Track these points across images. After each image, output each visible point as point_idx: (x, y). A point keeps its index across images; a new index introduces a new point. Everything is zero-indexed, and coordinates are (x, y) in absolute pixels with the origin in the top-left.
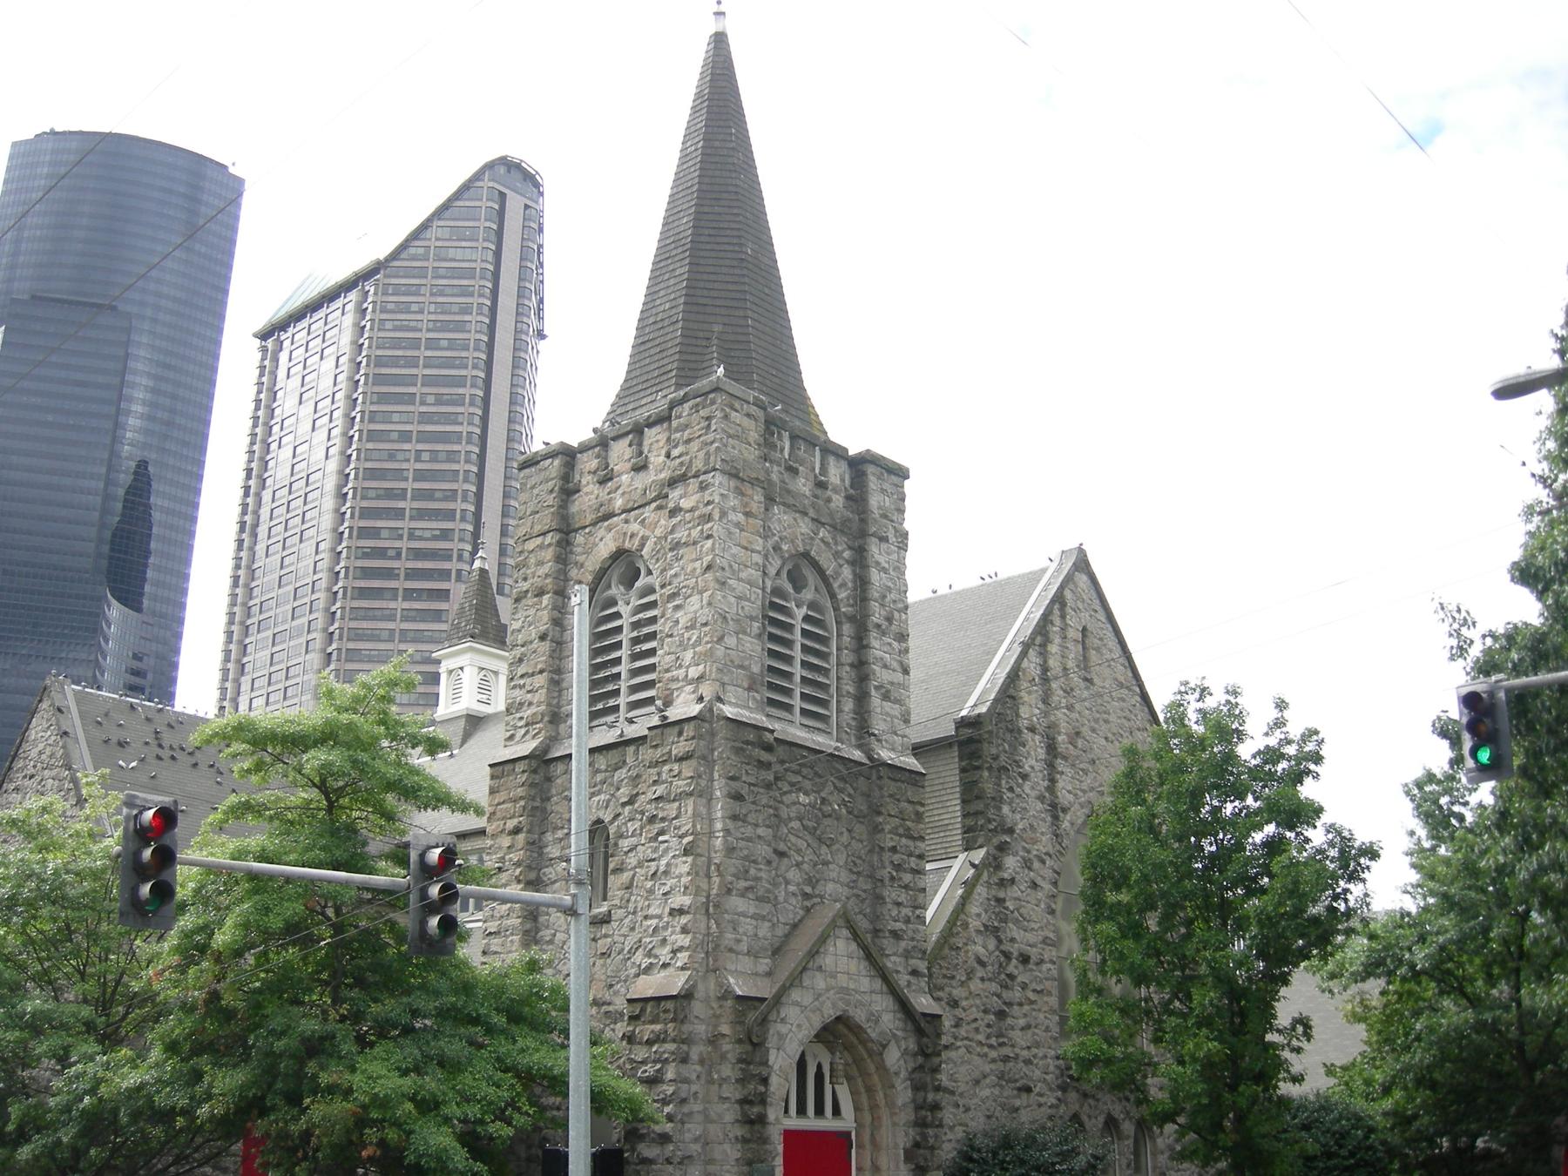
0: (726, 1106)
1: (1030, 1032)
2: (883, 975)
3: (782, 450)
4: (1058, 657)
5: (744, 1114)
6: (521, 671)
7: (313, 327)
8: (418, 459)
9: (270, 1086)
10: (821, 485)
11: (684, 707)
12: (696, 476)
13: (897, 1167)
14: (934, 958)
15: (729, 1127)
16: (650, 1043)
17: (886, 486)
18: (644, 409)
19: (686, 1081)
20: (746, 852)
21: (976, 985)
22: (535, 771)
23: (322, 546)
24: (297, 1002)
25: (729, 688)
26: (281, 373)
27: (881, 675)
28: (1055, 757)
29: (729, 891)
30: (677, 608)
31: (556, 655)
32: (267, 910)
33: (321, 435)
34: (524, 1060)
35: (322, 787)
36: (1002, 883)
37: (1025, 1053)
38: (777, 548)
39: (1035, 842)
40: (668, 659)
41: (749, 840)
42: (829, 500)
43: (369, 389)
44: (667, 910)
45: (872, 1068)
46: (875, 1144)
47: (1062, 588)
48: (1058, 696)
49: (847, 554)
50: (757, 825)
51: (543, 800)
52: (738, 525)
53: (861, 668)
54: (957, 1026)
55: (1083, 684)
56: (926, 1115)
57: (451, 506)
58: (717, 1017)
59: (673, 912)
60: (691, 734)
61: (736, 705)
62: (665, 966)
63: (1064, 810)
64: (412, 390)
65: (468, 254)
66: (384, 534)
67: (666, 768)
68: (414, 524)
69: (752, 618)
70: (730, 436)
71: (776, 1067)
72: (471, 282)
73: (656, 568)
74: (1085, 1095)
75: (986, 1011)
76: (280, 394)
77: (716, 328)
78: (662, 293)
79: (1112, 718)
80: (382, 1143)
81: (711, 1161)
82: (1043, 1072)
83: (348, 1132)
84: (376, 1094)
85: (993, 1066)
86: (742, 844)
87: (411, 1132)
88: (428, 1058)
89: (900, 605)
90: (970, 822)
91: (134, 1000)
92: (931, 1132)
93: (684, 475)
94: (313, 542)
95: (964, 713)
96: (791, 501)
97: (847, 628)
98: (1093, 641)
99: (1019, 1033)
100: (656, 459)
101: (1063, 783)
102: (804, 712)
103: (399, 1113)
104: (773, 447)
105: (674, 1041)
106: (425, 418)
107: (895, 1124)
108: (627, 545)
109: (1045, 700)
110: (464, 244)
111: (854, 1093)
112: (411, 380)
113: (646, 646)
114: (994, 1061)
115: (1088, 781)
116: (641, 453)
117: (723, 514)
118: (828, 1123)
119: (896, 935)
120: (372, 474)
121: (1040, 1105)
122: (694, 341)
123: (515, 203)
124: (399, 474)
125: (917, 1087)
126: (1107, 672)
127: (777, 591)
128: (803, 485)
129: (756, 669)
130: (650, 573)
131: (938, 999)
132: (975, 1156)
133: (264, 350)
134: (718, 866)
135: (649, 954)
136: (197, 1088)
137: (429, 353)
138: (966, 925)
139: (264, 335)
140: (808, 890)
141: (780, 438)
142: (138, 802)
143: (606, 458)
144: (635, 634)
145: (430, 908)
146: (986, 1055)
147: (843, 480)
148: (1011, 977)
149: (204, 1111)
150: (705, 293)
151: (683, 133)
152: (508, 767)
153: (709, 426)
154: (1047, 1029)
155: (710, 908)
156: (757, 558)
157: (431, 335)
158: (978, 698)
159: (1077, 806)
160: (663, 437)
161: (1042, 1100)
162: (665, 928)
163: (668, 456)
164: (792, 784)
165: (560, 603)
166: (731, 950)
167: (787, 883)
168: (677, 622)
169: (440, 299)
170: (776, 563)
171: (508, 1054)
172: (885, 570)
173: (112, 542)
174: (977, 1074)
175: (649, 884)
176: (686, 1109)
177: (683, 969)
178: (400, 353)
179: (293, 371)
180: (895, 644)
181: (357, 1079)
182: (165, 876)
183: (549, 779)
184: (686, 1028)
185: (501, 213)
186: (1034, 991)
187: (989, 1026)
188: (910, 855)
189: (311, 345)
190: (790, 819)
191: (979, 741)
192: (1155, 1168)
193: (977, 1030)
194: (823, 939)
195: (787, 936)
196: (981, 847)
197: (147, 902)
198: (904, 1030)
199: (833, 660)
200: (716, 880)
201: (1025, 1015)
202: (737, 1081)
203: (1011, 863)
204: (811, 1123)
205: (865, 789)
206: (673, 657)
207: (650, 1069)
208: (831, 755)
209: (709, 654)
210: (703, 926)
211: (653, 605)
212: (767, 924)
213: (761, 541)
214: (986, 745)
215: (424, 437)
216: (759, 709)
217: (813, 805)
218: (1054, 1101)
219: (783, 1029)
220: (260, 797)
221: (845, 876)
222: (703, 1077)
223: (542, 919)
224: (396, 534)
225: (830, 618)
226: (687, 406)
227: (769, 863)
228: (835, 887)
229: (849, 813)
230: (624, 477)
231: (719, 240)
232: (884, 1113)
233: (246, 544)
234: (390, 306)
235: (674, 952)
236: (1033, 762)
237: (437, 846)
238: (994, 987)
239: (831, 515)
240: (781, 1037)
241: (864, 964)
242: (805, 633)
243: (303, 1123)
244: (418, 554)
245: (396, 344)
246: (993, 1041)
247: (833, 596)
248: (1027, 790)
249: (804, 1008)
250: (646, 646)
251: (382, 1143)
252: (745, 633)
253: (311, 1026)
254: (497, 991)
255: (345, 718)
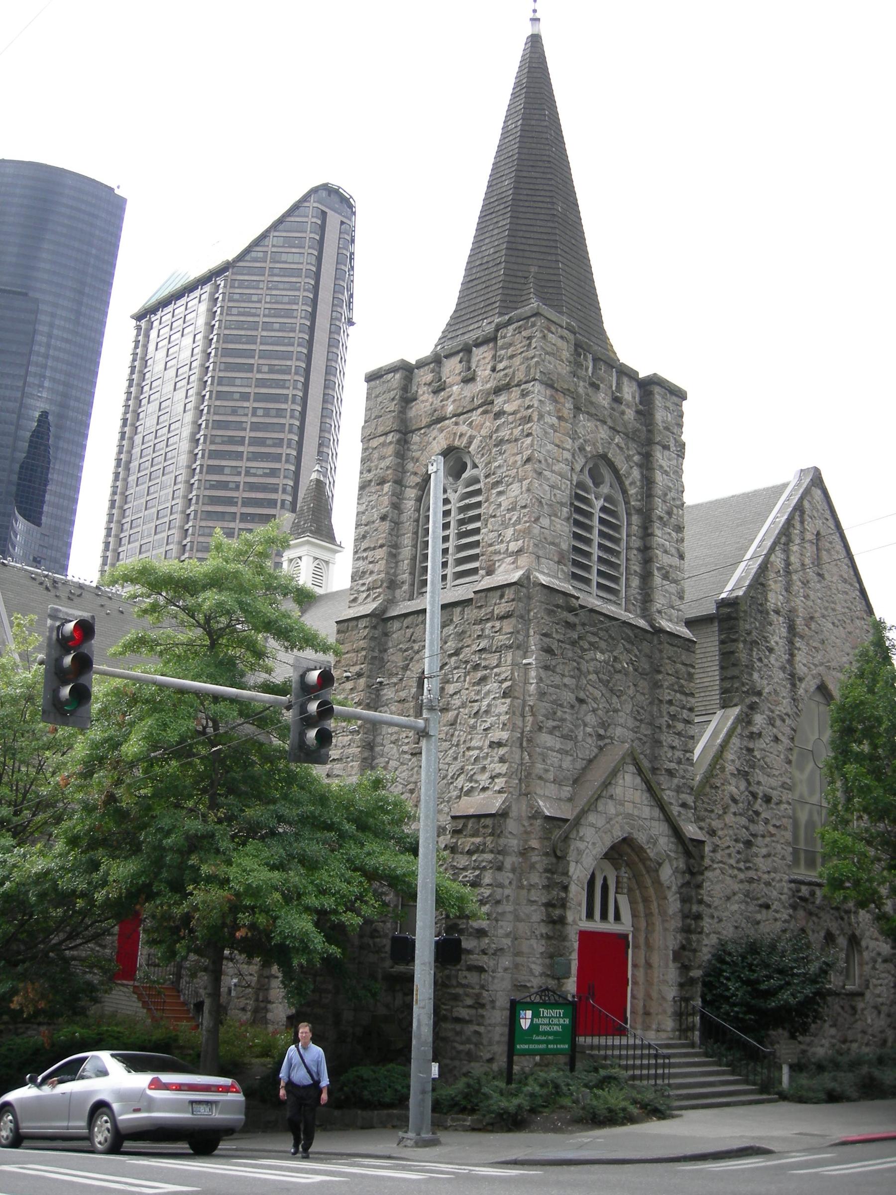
0: (534, 908)
1: (770, 859)
2: (662, 806)
3: (587, 369)
4: (797, 555)
5: (548, 915)
6: (364, 545)
7: (176, 312)
8: (254, 414)
9: (156, 875)
10: (617, 400)
11: (507, 573)
12: (518, 385)
13: (667, 966)
14: (698, 793)
15: (535, 926)
16: (470, 853)
17: (668, 404)
18: (472, 334)
19: (501, 886)
20: (554, 697)
21: (729, 819)
22: (375, 627)
23: (179, 479)
24: (177, 806)
25: (543, 560)
26: (151, 347)
27: (663, 559)
28: (794, 636)
29: (540, 729)
30: (500, 493)
31: (394, 533)
32: (165, 726)
33: (181, 394)
34: (371, 862)
35: (206, 624)
36: (752, 736)
37: (766, 876)
38: (582, 449)
39: (778, 704)
40: (491, 535)
41: (557, 687)
42: (623, 413)
43: (218, 360)
44: (487, 743)
45: (648, 882)
46: (649, 946)
47: (802, 499)
48: (797, 586)
49: (636, 458)
50: (563, 675)
51: (380, 651)
52: (552, 426)
53: (646, 551)
54: (714, 851)
55: (816, 578)
56: (691, 922)
57: (279, 450)
58: (526, 832)
59: (492, 745)
60: (512, 597)
61: (548, 575)
62: (484, 789)
63: (801, 680)
64: (251, 361)
65: (297, 258)
66: (227, 471)
67: (489, 625)
68: (250, 464)
69: (562, 504)
70: (547, 353)
71: (575, 877)
72: (299, 280)
73: (480, 461)
74: (811, 914)
75: (736, 841)
76: (149, 362)
77: (533, 269)
78: (487, 241)
79: (838, 607)
80: (253, 926)
81: (518, 954)
82: (779, 892)
83: (223, 916)
84: (249, 885)
85: (741, 886)
86: (552, 690)
87: (275, 918)
88: (291, 856)
89: (678, 503)
90: (727, 685)
91: (42, 805)
92: (694, 937)
93: (508, 384)
94: (173, 475)
95: (723, 596)
96: (593, 411)
97: (635, 519)
98: (825, 544)
99: (762, 860)
100: (483, 372)
101: (800, 657)
102: (600, 586)
103: (269, 901)
104: (579, 365)
105: (492, 852)
106: (261, 383)
107: (665, 930)
108: (456, 443)
109: (788, 590)
110: (294, 250)
111: (632, 902)
112: (250, 354)
113: (470, 527)
114: (741, 881)
115: (819, 657)
116: (469, 369)
117: (541, 417)
118: (610, 927)
119: (670, 773)
120: (218, 425)
121: (776, 920)
122: (514, 279)
123: (333, 220)
124: (240, 426)
125: (685, 900)
126: (835, 570)
127: (580, 485)
128: (603, 399)
129: (564, 546)
130: (475, 466)
131: (701, 828)
132: (728, 959)
133: (139, 328)
134: (532, 707)
135: (471, 779)
136: (94, 875)
137: (265, 333)
138: (723, 769)
139: (139, 317)
140: (602, 732)
141: (586, 359)
142: (61, 616)
143: (439, 373)
144: (462, 516)
145: (307, 721)
146: (736, 876)
147: (634, 397)
148: (757, 813)
149: (99, 896)
150: (524, 241)
151: (505, 114)
152: (351, 624)
153: (529, 345)
154: (783, 858)
155: (525, 742)
156: (567, 455)
157: (266, 320)
158: (734, 584)
159: (810, 677)
160: (489, 355)
161: (778, 916)
162: (485, 758)
163: (494, 370)
164: (591, 644)
165: (398, 491)
166: (540, 778)
167: (585, 725)
168: (500, 505)
169: (274, 292)
170: (581, 461)
171: (357, 856)
172: (666, 473)
173: (20, 473)
174: (728, 892)
175: (472, 721)
176: (500, 909)
177: (500, 792)
178: (242, 332)
179: (160, 345)
180: (674, 534)
181: (232, 872)
182: (82, 680)
183: (386, 634)
184: (502, 841)
185: (323, 227)
186: (774, 826)
187: (739, 852)
188: (683, 708)
189: (175, 325)
190: (589, 672)
191: (736, 619)
192: (861, 976)
193: (730, 855)
194: (614, 773)
195: (584, 769)
196: (736, 705)
197: (67, 702)
198: (676, 852)
199: (624, 544)
200: (529, 719)
201: (767, 846)
202: (544, 887)
203: (759, 719)
204: (597, 926)
205: (647, 651)
206: (496, 534)
207: (470, 875)
208: (624, 622)
209: (527, 532)
210: (517, 757)
211: (478, 492)
212: (570, 758)
213: (570, 441)
214: (741, 622)
215: (259, 397)
216: (565, 580)
217: (606, 662)
218: (787, 917)
219: (581, 845)
220: (153, 635)
221: (631, 723)
222: (514, 883)
223: (378, 749)
224: (236, 471)
225: (622, 509)
226: (511, 328)
227: (572, 707)
228: (623, 732)
229: (636, 670)
230: (455, 388)
231: (535, 199)
232: (657, 920)
233: (121, 476)
234: (236, 297)
235: (492, 778)
236: (777, 639)
237: (315, 669)
238: (743, 821)
239: (625, 425)
240: (580, 852)
241: (646, 795)
242: (602, 521)
243: (185, 907)
244: (252, 487)
245: (240, 325)
246: (742, 865)
247: (624, 492)
248: (773, 661)
249: (598, 829)
250: (470, 527)
251: (253, 926)
252: (556, 516)
253: (194, 825)
254: (347, 805)
255: (232, 567)
